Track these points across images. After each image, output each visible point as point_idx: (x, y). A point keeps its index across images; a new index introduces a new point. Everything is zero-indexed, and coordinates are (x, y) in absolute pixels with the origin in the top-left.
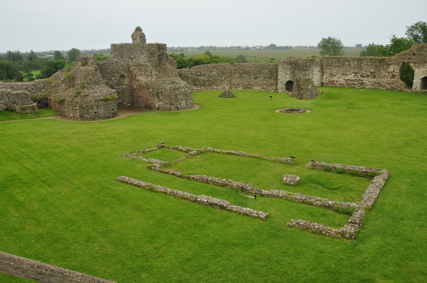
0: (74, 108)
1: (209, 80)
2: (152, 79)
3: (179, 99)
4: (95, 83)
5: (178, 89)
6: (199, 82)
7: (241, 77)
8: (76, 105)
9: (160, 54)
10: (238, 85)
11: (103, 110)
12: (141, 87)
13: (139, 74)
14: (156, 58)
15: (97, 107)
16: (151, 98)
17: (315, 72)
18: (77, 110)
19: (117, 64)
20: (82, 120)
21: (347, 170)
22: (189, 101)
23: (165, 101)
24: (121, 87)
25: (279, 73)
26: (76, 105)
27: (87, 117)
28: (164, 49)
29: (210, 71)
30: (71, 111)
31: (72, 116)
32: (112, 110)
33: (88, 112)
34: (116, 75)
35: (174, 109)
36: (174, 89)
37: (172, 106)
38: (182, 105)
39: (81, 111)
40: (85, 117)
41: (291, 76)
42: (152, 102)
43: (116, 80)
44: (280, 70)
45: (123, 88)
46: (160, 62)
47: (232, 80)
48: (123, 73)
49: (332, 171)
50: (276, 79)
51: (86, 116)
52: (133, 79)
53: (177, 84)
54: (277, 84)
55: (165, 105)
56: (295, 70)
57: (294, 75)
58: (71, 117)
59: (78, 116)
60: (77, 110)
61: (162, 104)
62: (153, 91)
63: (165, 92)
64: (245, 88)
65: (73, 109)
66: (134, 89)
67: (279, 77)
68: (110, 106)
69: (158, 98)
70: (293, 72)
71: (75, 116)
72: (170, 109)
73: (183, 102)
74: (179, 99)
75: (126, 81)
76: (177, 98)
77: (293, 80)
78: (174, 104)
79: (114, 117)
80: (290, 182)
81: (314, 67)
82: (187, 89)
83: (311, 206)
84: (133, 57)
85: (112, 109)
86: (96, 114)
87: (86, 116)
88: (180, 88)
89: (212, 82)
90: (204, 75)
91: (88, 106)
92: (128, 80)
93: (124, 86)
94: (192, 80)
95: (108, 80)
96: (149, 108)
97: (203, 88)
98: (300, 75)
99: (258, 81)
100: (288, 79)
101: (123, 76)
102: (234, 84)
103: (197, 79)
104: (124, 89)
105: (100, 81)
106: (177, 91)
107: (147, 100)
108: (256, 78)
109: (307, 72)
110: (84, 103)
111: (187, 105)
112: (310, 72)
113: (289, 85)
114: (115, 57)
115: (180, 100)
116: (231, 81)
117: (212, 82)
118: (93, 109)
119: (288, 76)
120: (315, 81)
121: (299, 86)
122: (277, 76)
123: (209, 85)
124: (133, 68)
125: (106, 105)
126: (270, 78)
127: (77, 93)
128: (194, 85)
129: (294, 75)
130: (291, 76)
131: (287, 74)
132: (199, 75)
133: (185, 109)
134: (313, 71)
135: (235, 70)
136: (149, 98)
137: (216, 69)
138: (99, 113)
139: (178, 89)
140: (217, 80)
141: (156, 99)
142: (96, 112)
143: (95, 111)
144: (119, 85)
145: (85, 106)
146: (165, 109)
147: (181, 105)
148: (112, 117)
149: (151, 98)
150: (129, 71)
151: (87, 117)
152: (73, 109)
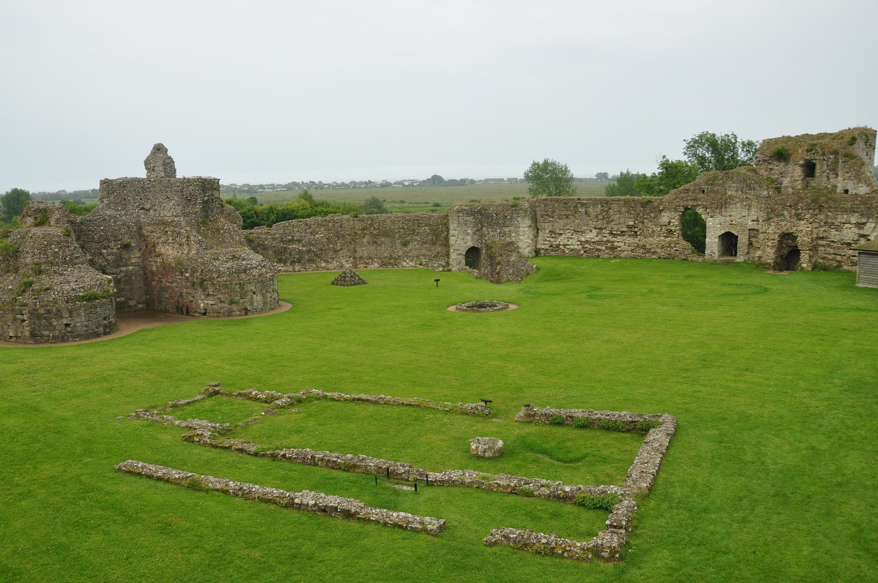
0: (19, 316)
1: (309, 251)
2: (189, 251)
3: (247, 291)
4: (65, 262)
5: (245, 271)
6: (290, 254)
7: (375, 242)
8: (21, 311)
9: (206, 198)
10: (370, 258)
11: (83, 319)
12: (167, 269)
13: (163, 242)
14: (198, 208)
15: (71, 312)
16: (189, 290)
17: (521, 229)
18: (24, 321)
19: (115, 222)
20: (36, 342)
21: (595, 420)
22: (269, 295)
23: (219, 296)
24: (124, 269)
25: (452, 232)
26: (21, 311)
27: (49, 336)
28: (215, 189)
29: (311, 233)
30: (9, 324)
31: (11, 335)
32: (105, 319)
33: (50, 324)
34: (112, 245)
35: (238, 313)
36: (238, 272)
37: (234, 307)
38: (255, 304)
39: (34, 323)
40: (42, 336)
41: (476, 237)
42: (191, 298)
43: (112, 254)
44: (452, 227)
45: (127, 271)
46: (207, 217)
47: (358, 249)
48: (126, 240)
49: (567, 425)
50: (446, 244)
51: (46, 333)
52: (150, 253)
53: (244, 260)
54: (448, 255)
55: (219, 305)
56: (482, 226)
57: (482, 236)
58: (11, 337)
59: (27, 334)
60: (24, 321)
61: (213, 302)
62: (192, 275)
63: (218, 277)
64: (384, 265)
65: (15, 319)
66: (153, 273)
67: (452, 240)
68: (99, 309)
69: (204, 290)
70: (478, 230)
71: (19, 334)
72: (230, 314)
73: (258, 298)
74: (247, 291)
75: (135, 257)
76: (243, 289)
77: (479, 246)
78: (237, 303)
79: (109, 333)
80: (484, 452)
81: (519, 219)
82: (264, 270)
83: (531, 499)
84: (148, 206)
85: (104, 316)
86: (69, 329)
87: (46, 333)
88: (249, 269)
89: (316, 255)
90: (299, 241)
91: (49, 312)
92: (138, 255)
93: (131, 268)
94: (275, 252)
95: (94, 254)
96: (185, 312)
97: (297, 267)
98: (492, 235)
99: (411, 250)
100: (470, 244)
101: (126, 247)
102: (361, 257)
103: (285, 248)
104: (129, 274)
105: (76, 258)
106: (243, 276)
107: (181, 295)
108: (405, 244)
109: (506, 229)
110: (42, 306)
111: (265, 303)
112: (512, 228)
113: (472, 256)
114: (110, 208)
115: (250, 294)
116: (355, 251)
117: (316, 255)
118: (61, 317)
119: (469, 238)
120: (524, 246)
121: (491, 257)
122: (447, 239)
123: (311, 261)
124: (149, 228)
125: (91, 308)
126: (434, 243)
127: (25, 283)
128: (280, 261)
129: (482, 236)
130: (476, 237)
131: (468, 234)
132: (290, 241)
133: (262, 311)
134: (519, 227)
135: (363, 229)
136: (185, 290)
137: (323, 229)
138: (75, 326)
139: (245, 271)
140: (326, 250)
141: (199, 294)
142: (67, 325)
143: (65, 322)
144: (119, 266)
145: (42, 311)
146: (218, 314)
147: (252, 304)
148: (105, 334)
149: (189, 290)
150: (141, 235)
151: (49, 336)
152: (15, 319)
